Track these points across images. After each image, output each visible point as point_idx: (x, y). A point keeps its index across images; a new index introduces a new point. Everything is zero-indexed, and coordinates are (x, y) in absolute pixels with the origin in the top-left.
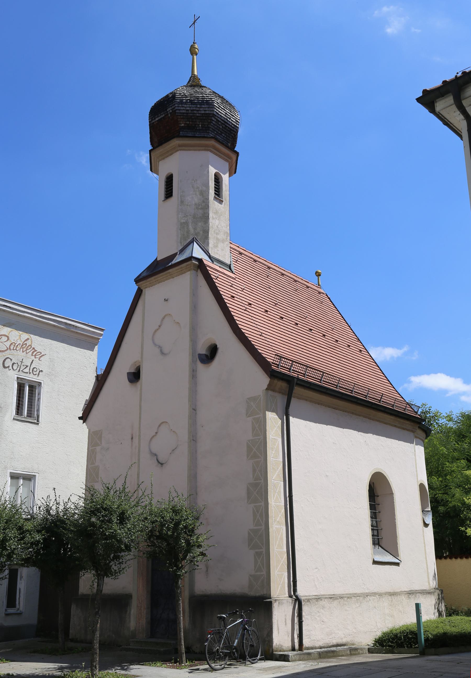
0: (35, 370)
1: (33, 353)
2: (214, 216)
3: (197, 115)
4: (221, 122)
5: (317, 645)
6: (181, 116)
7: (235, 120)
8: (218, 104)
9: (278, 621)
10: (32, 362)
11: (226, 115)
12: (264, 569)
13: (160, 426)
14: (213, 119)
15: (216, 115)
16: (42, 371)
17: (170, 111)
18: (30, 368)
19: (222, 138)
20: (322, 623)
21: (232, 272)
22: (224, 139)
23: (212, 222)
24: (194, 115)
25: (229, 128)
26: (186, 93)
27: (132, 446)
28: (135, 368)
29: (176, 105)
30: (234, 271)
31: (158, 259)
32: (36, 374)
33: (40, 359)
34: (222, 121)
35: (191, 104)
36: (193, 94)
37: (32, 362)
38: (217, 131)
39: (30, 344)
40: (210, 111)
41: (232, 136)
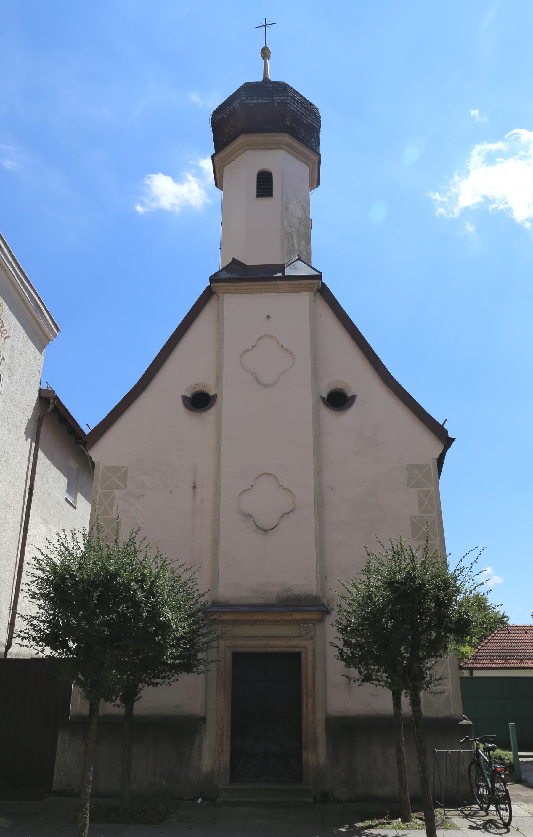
3: (304, 121)
6: (290, 112)
13: (263, 474)
24: (302, 119)
28: (193, 392)
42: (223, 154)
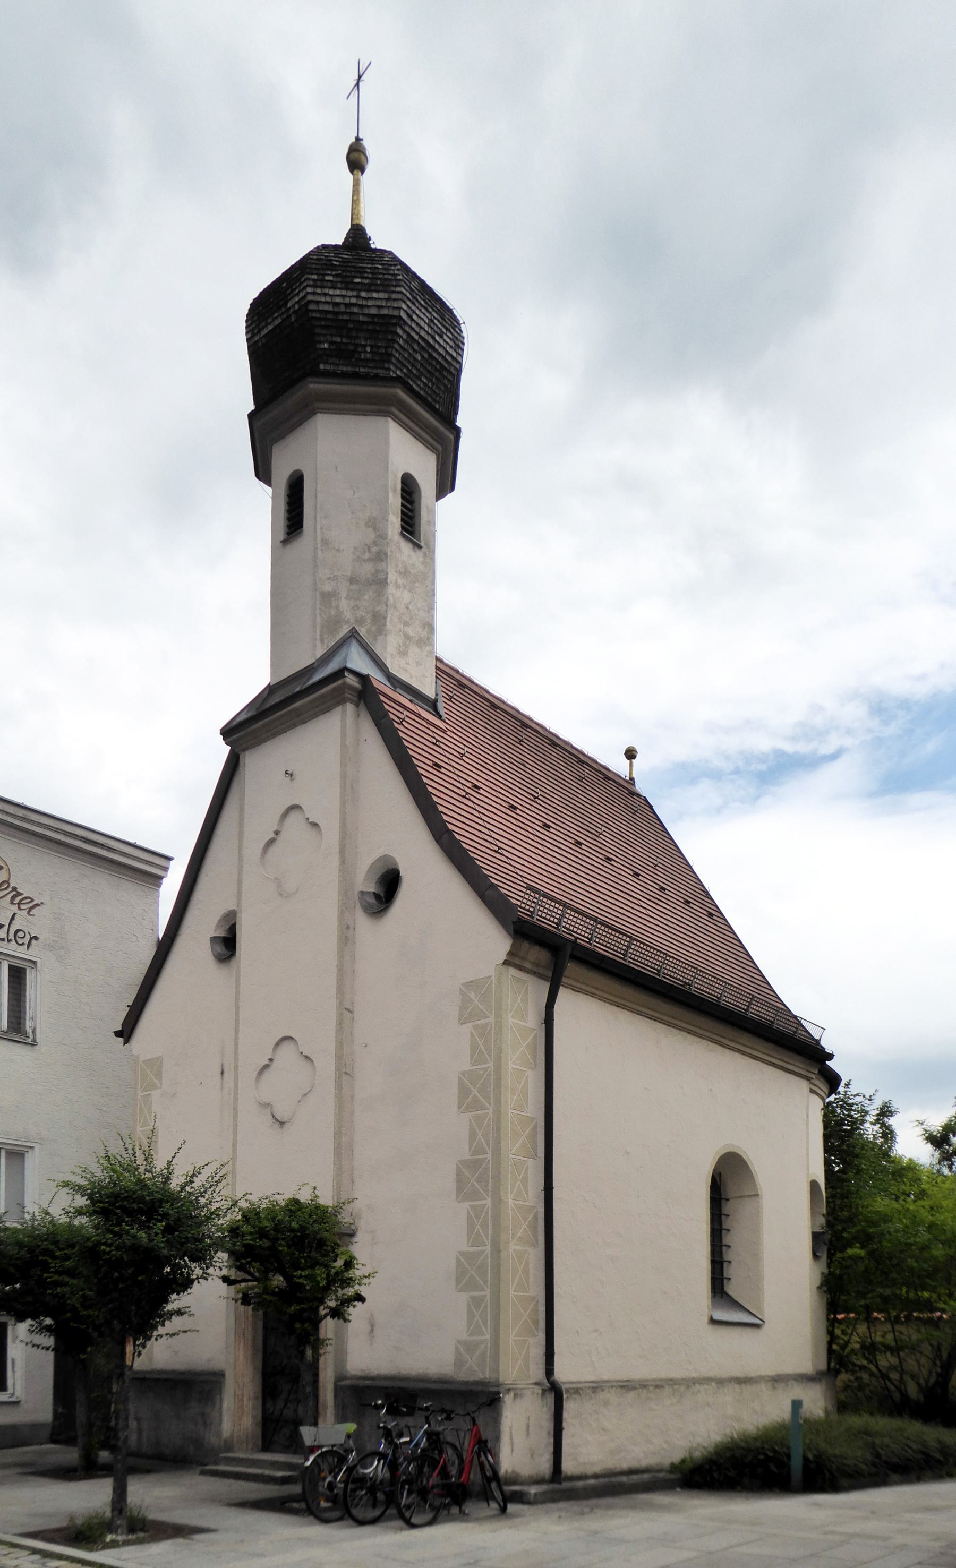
0: (21, 934)
1: (13, 898)
2: (400, 581)
3: (361, 318)
4: (419, 344)
5: (590, 1470)
7: (455, 343)
8: (412, 293)
9: (511, 1428)
10: (13, 918)
11: (432, 325)
12: (486, 1328)
14: (399, 331)
15: (405, 323)
16: (36, 938)
17: (293, 305)
18: (8, 930)
19: (421, 388)
20: (602, 1431)
21: (440, 717)
22: (425, 391)
23: (393, 595)
24: (354, 318)
25: (437, 360)
26: (332, 258)
27: (222, 1088)
29: (309, 290)
30: (444, 716)
31: (271, 684)
32: (23, 944)
33: (31, 913)
34: (420, 341)
35: (346, 289)
36: (351, 262)
37: (13, 918)
38: (410, 367)
39: (7, 880)
40: (391, 309)
41: (445, 386)
42: (276, 410)
